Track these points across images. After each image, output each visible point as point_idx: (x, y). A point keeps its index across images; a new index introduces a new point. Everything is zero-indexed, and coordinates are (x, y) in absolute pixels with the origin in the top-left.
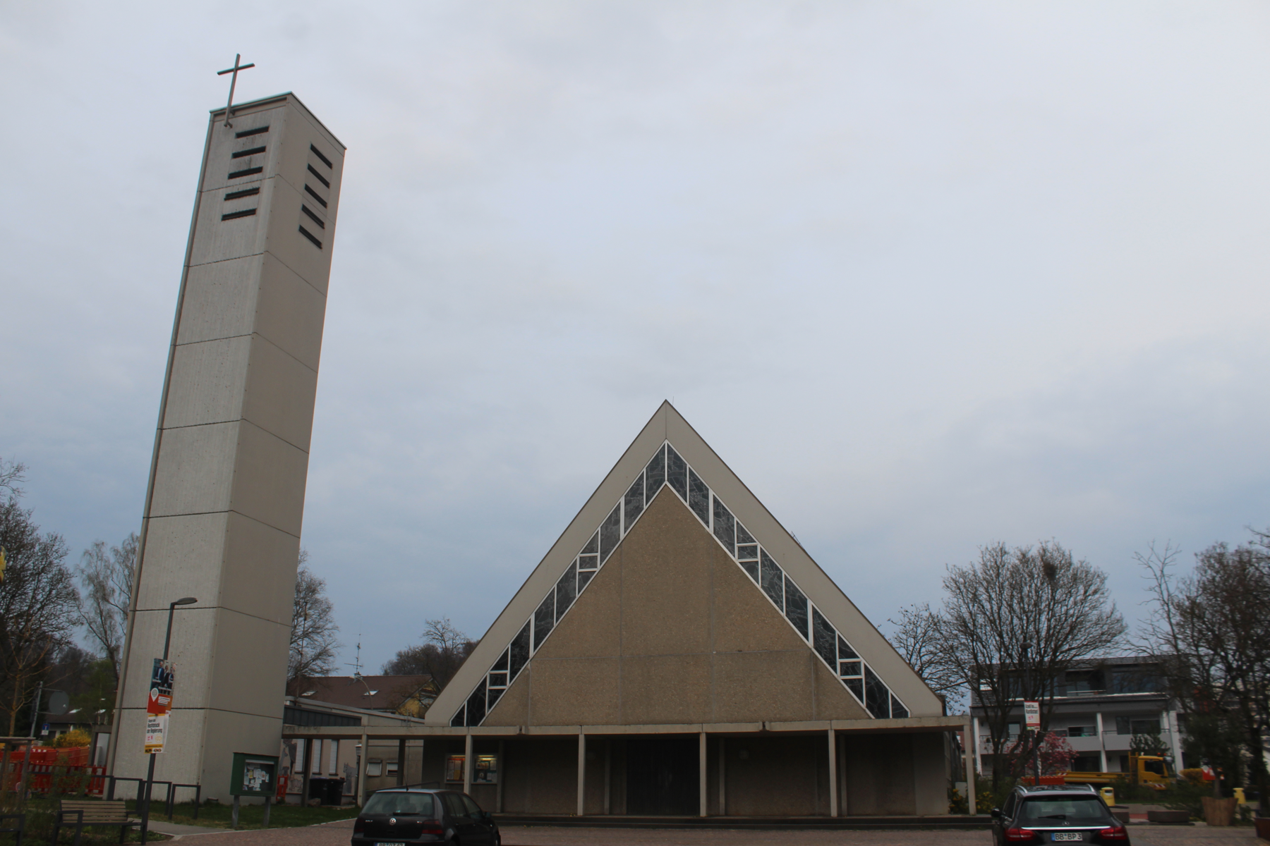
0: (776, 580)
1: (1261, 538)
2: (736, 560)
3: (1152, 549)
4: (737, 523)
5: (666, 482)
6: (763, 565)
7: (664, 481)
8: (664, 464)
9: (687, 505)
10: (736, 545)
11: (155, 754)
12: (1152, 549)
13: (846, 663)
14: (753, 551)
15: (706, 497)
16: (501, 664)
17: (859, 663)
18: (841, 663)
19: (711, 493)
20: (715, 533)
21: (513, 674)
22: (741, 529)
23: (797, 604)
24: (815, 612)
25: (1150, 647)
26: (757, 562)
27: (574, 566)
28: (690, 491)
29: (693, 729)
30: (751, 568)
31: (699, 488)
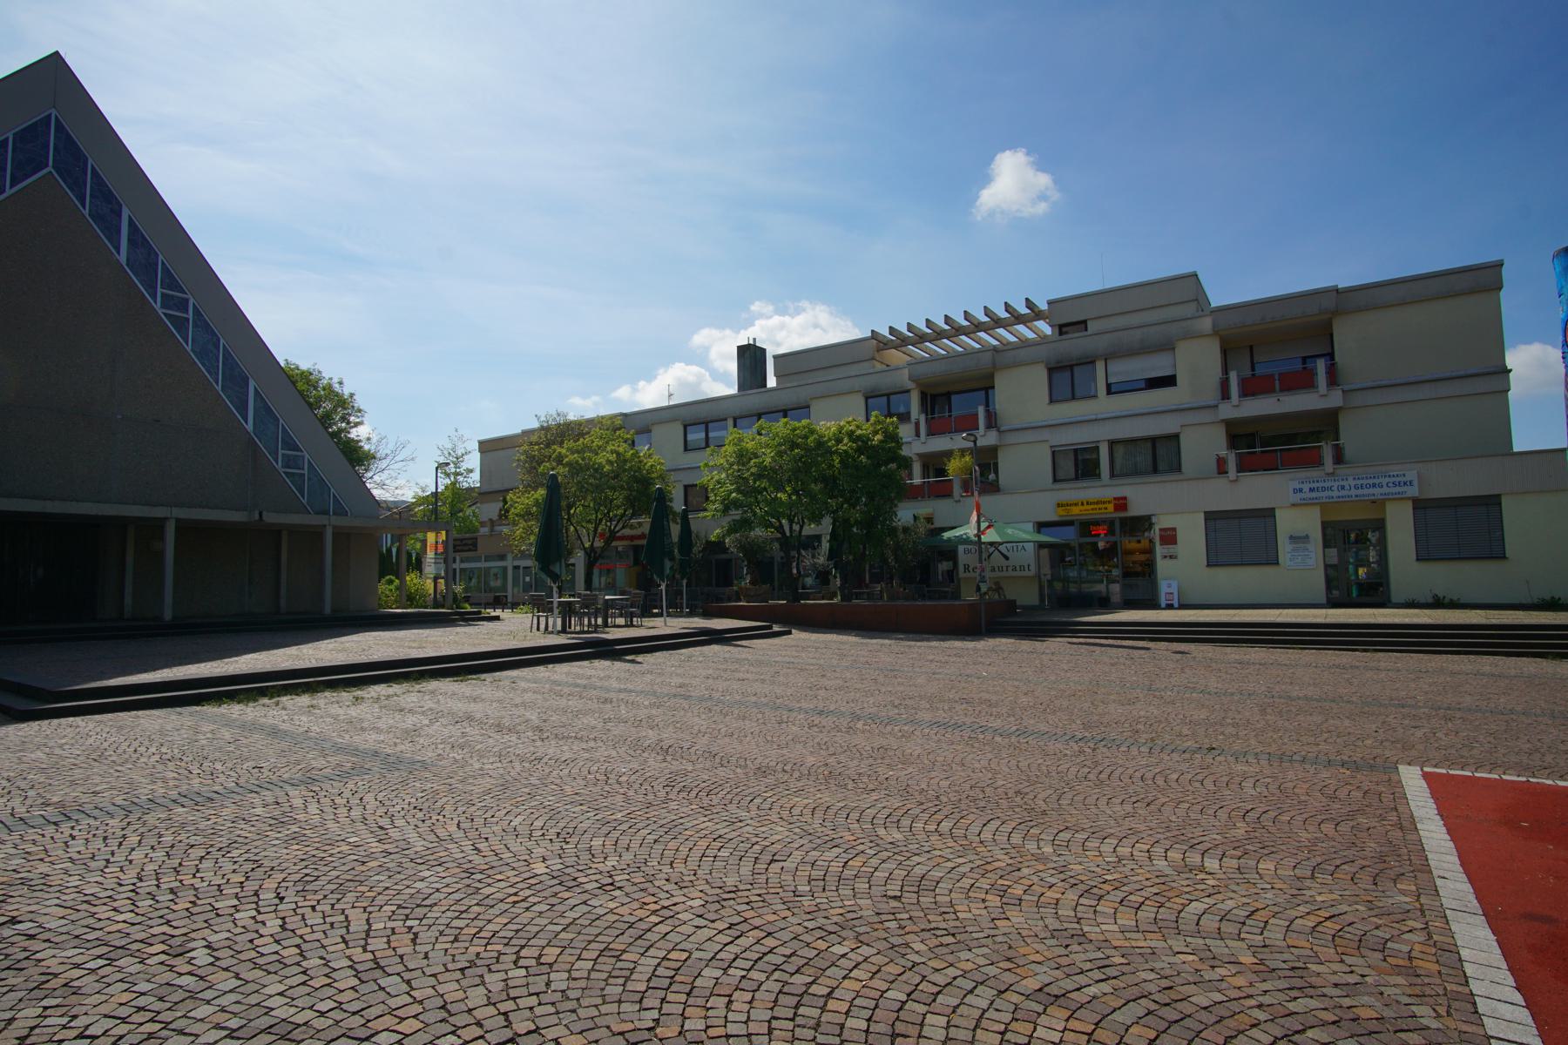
0: (1434, 763)
1: (517, 1005)
2: (158, 306)
3: (1189, 1016)
4: (163, 263)
6: (195, 325)
7: (47, 165)
8: (49, 141)
11: (993, 451)
12: (1189, 1016)
13: (288, 456)
14: (183, 305)
15: (120, 215)
17: (303, 457)
18: (283, 455)
20: (128, 265)
23: (236, 380)
25: (99, 1017)
26: (188, 320)
28: (91, 195)
29: (159, 512)
30: (181, 324)
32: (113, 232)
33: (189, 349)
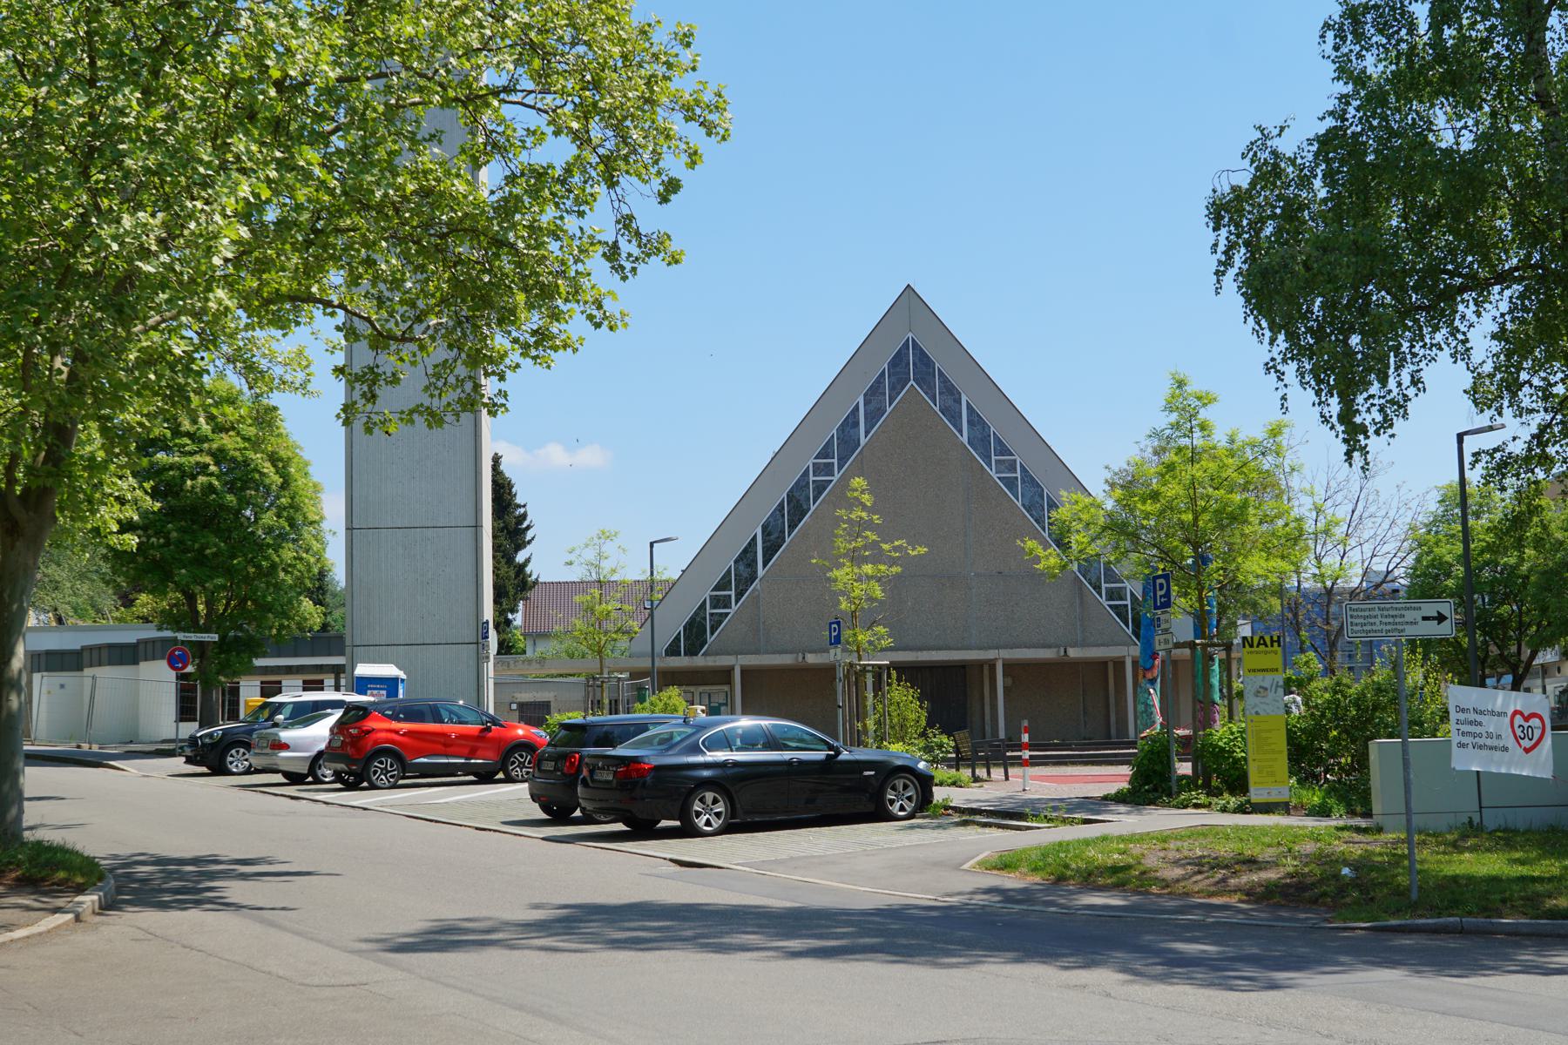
2: (993, 473)
5: (912, 382)
9: (937, 409)
10: (1128, 602)
16: (723, 584)
19: (964, 398)
21: (739, 595)
22: (998, 441)
24: (969, 406)
27: (806, 472)
30: (1010, 483)
31: (950, 391)
32: (955, 418)
33: (1019, 504)
